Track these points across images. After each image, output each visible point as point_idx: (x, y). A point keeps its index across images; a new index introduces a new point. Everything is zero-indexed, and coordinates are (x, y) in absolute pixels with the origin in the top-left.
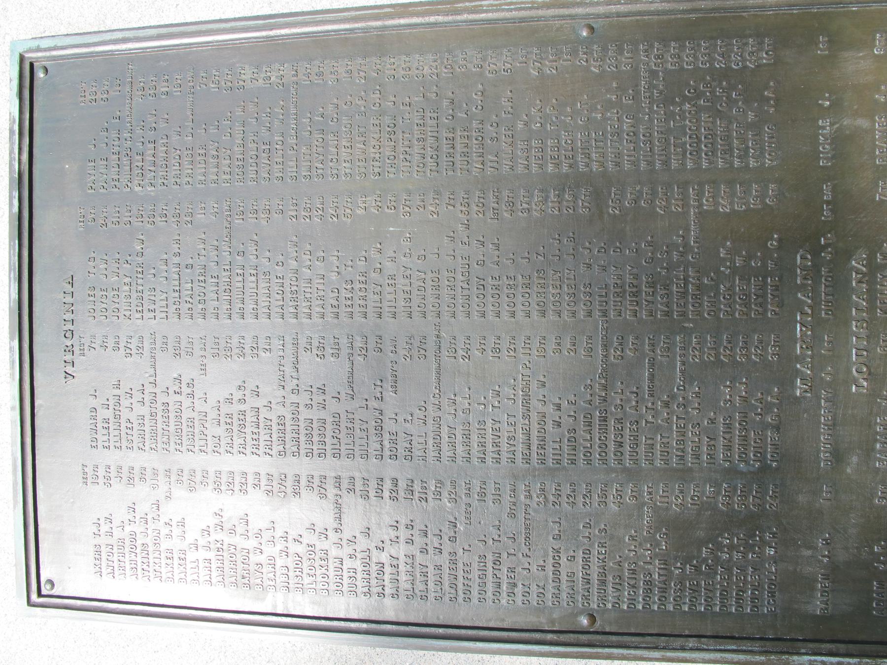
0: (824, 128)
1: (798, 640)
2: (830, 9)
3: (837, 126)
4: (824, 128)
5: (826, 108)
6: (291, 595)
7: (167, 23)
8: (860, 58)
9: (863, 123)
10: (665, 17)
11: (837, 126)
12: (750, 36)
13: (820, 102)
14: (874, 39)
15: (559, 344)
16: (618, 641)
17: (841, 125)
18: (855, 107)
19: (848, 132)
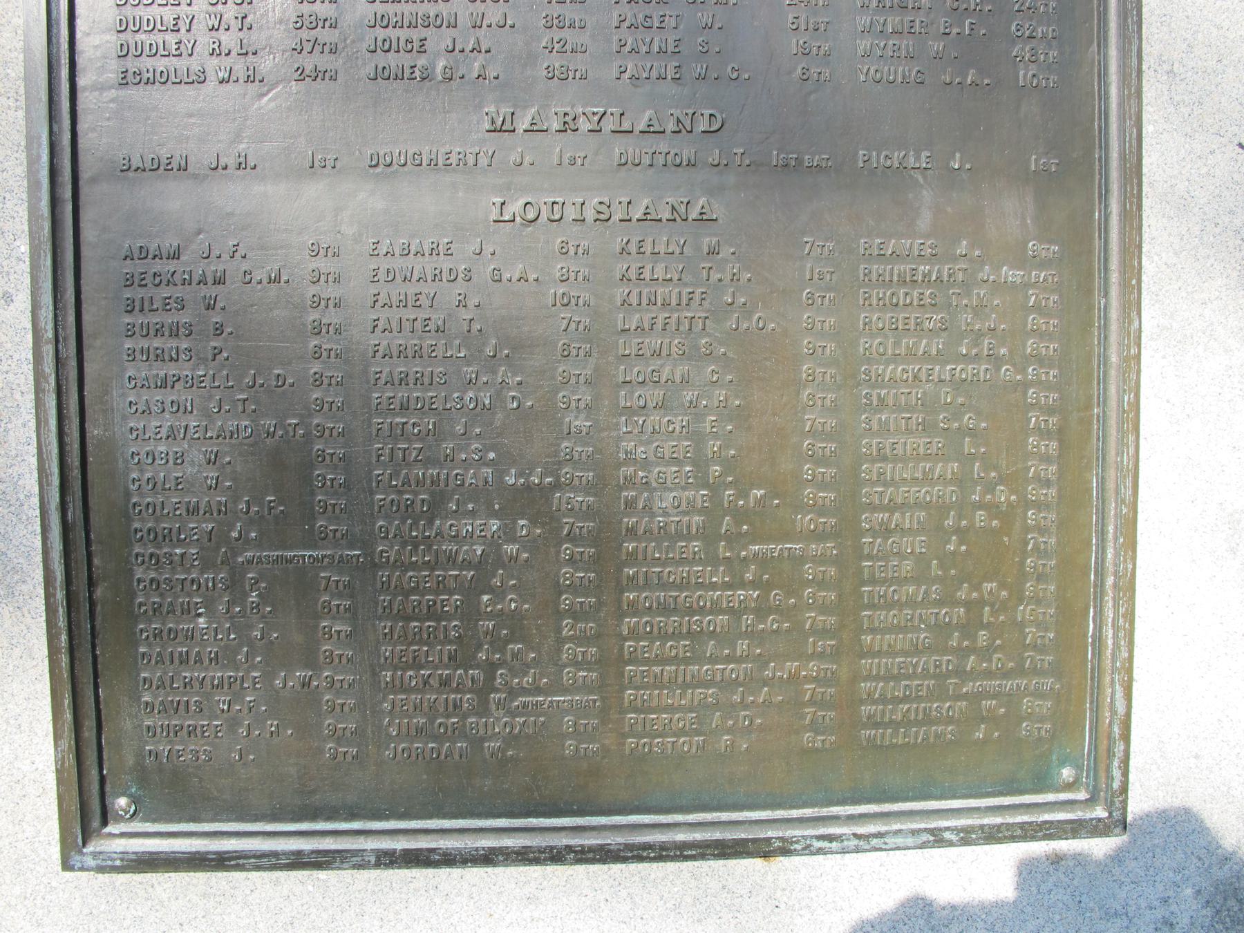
0: (918, 158)
1: (93, 627)
2: (1097, 177)
3: (921, 180)
4: (918, 158)
5: (948, 164)
6: (112, 38)
7: (1141, 464)
8: (1024, 219)
9: (925, 221)
10: (1110, 642)
11: (921, 180)
12: (1061, 53)
13: (958, 155)
14: (1050, 242)
15: (572, 26)
16: (59, 61)
17: (922, 186)
18: (949, 209)
19: (911, 196)
